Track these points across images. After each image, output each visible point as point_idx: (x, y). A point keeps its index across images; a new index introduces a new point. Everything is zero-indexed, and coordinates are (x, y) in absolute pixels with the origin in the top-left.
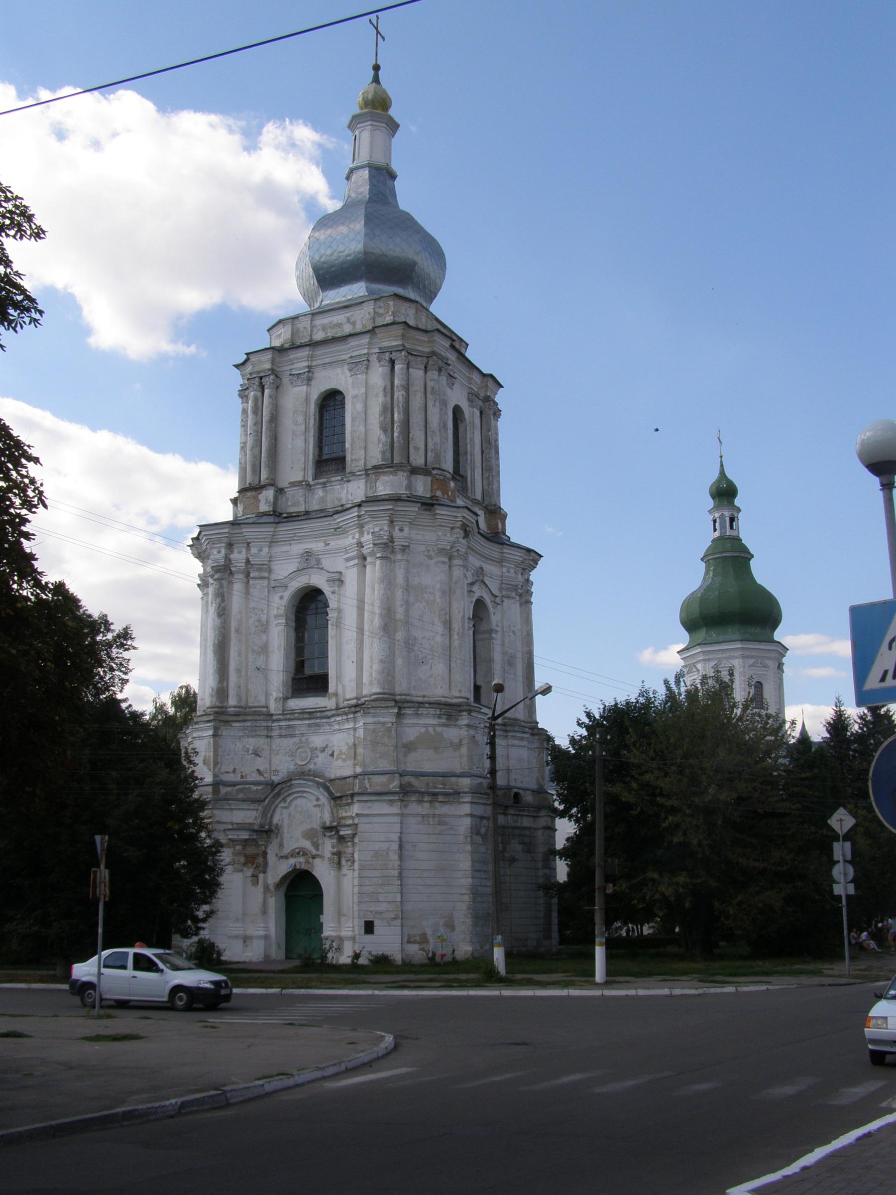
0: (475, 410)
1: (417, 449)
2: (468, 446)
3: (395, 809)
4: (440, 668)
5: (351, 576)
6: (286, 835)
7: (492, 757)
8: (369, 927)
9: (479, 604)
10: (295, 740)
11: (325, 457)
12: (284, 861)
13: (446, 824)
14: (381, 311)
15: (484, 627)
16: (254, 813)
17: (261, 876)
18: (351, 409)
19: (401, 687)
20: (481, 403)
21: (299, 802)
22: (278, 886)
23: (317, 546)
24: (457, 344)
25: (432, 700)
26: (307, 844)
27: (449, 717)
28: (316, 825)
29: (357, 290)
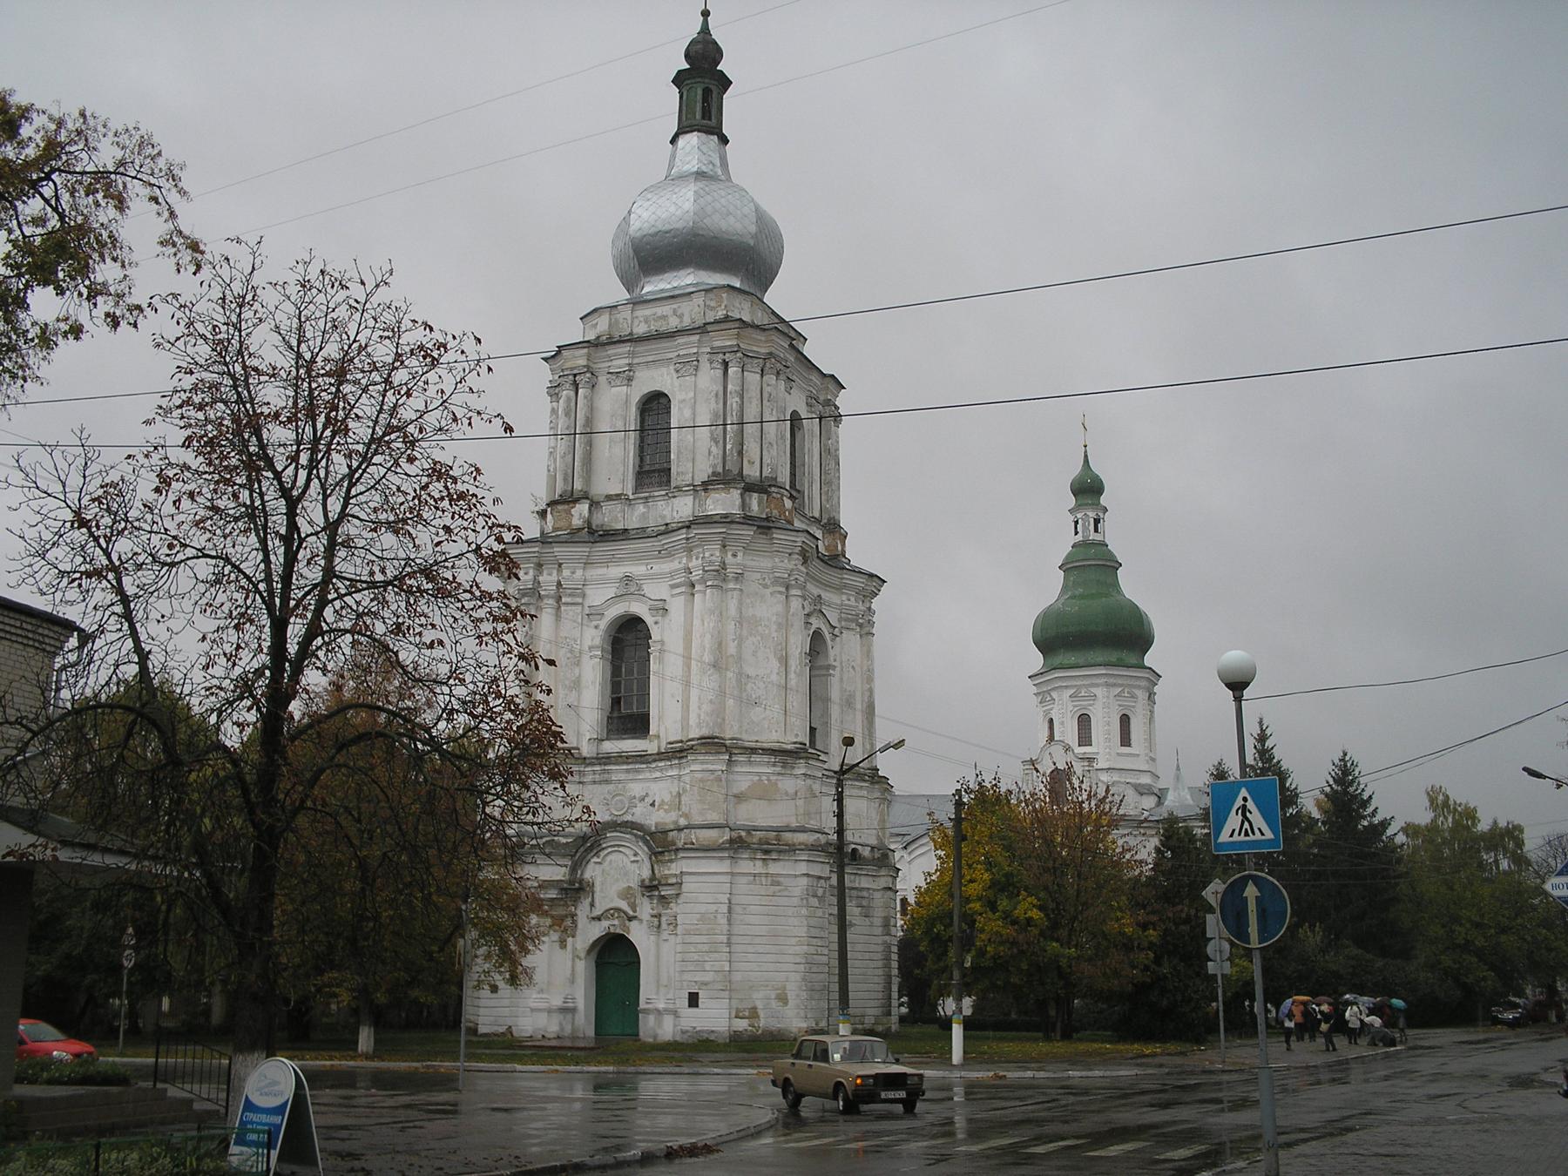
1: (751, 463)
3: (725, 867)
4: (776, 710)
5: (677, 605)
7: (840, 815)
8: (693, 1000)
9: (817, 637)
10: (611, 787)
11: (647, 468)
12: (597, 923)
13: (778, 884)
14: (713, 304)
15: (821, 662)
17: (570, 940)
22: (589, 952)
23: (638, 570)
24: (794, 339)
25: (765, 745)
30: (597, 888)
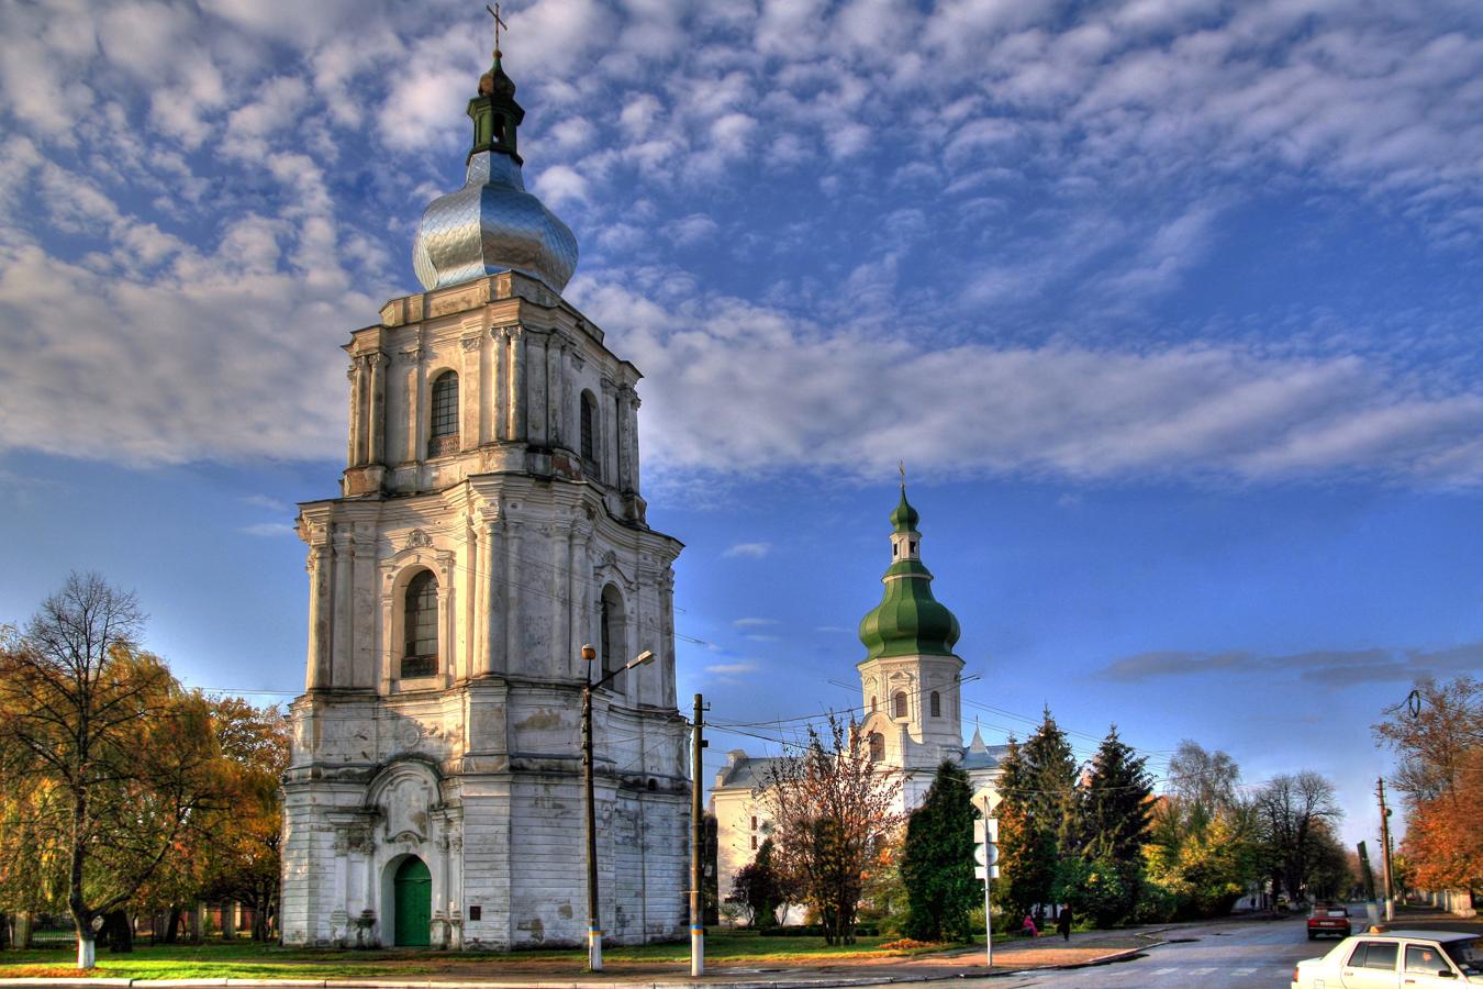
0: (609, 396)
2: (601, 432)
6: (393, 819)
16: (359, 796)
18: (466, 388)
19: (513, 667)
20: (617, 390)
21: (406, 784)
26: (415, 828)
27: (567, 696)
28: (423, 807)
29: (476, 268)
30: (392, 812)
